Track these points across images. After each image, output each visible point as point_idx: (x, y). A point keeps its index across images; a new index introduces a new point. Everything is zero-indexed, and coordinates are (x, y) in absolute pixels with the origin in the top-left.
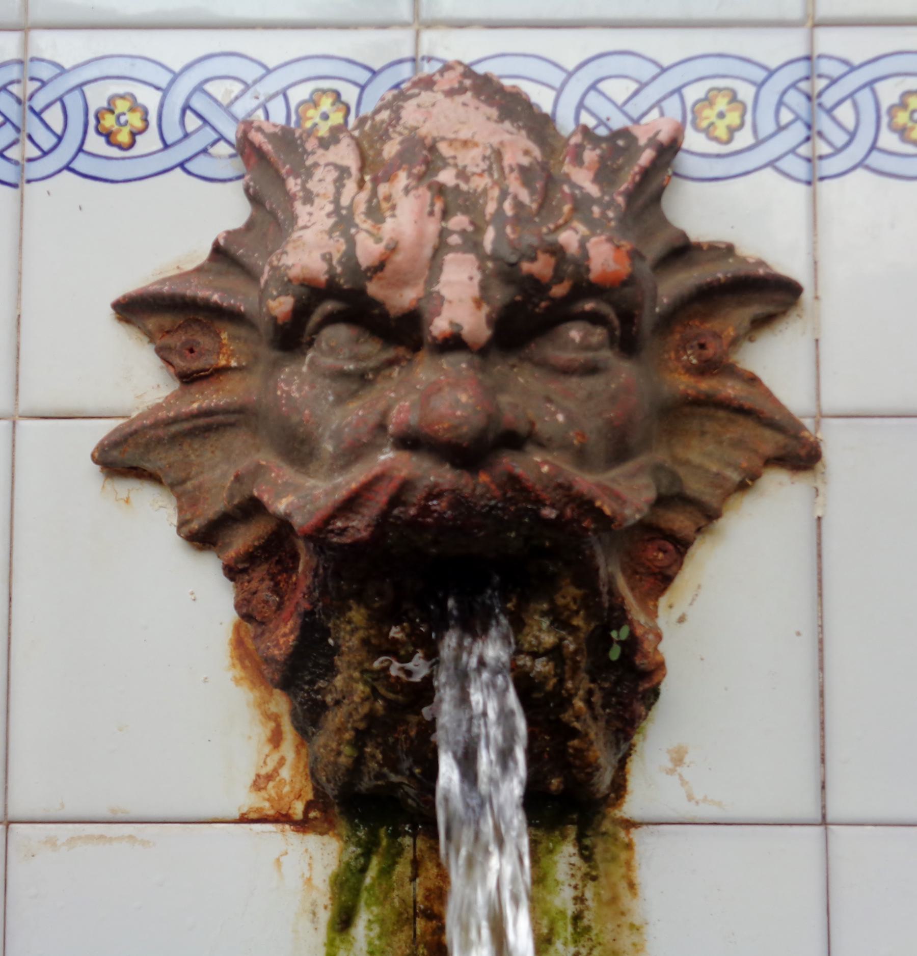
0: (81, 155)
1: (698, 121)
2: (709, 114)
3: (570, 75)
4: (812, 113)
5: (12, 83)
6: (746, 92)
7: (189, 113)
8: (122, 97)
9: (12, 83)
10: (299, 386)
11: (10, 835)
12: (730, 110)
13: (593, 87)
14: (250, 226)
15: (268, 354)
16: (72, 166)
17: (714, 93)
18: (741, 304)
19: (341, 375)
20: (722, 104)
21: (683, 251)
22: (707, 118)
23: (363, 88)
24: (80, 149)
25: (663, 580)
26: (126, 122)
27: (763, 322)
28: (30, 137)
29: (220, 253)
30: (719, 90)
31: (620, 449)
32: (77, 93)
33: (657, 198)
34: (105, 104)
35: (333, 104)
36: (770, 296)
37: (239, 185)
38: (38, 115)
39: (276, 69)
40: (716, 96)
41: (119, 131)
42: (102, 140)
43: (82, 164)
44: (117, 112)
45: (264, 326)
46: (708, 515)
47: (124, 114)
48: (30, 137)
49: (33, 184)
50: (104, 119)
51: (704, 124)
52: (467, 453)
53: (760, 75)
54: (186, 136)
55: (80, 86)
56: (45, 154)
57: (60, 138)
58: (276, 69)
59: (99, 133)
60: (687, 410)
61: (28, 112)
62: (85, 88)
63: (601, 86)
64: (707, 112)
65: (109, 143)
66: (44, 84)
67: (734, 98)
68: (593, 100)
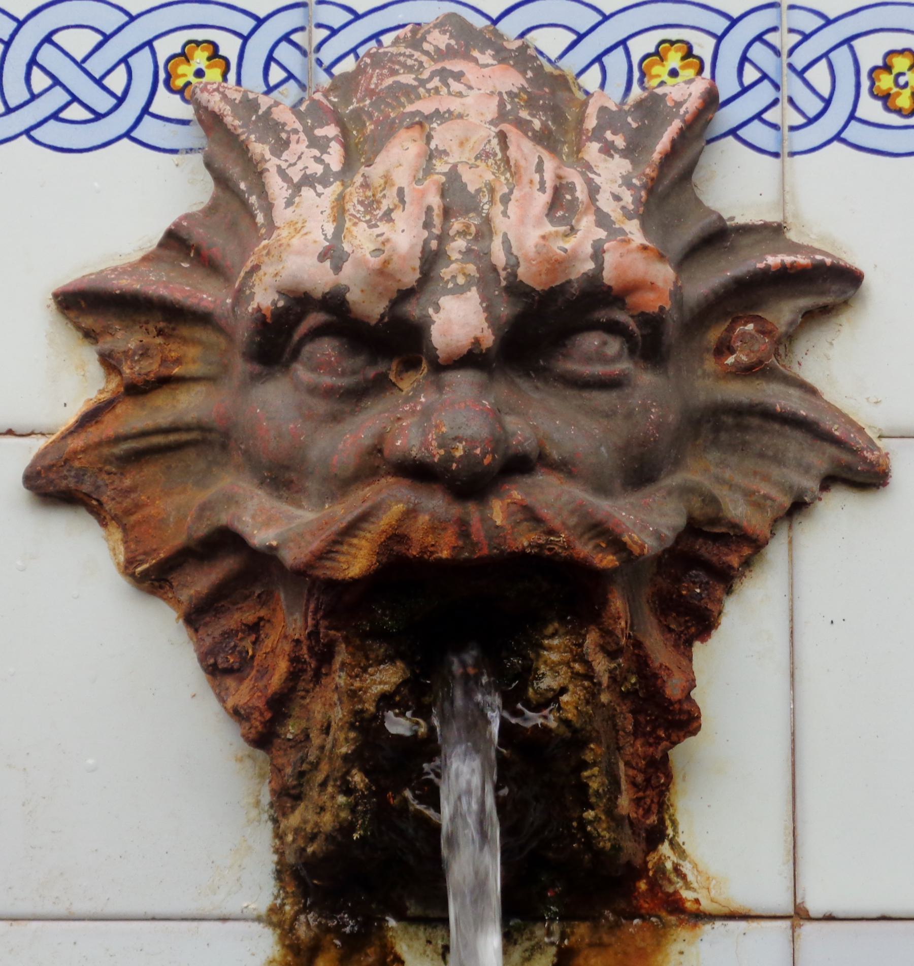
0: (853, 123)
1: (646, 80)
2: (186, 73)
3: (21, 24)
4: (308, 71)
5: (295, 31)
6: (229, 47)
7: (36, 70)
8: (902, 52)
9: (295, 31)
10: (276, 406)
11: (800, 943)
12: (684, 67)
13: (48, 39)
14: (212, 209)
15: (241, 367)
16: (843, 135)
17: (667, 45)
18: (793, 296)
19: (329, 393)
20: (200, 58)
21: (719, 237)
22: (184, 75)
23: (246, 39)
24: (852, 117)
25: (703, 623)
26: (906, 85)
27: (816, 316)
28: (791, 101)
29: (176, 241)
30: (198, 43)
31: (640, 470)
32: (845, 48)
33: (687, 175)
34: (880, 63)
35: (684, 58)
36: (829, 287)
37: (197, 159)
38: (801, 74)
39: (613, 15)
40: (669, 50)
41: (898, 94)
42: (879, 104)
43: (855, 132)
44: (895, 71)
45: (243, 332)
46: (753, 546)
47: (902, 74)
48: (791, 101)
49: (797, 157)
50: (880, 80)
51: (179, 83)
52: (466, 483)
53: (720, 25)
54: (34, 97)
55: (848, 41)
56: (811, 121)
57: (828, 102)
58: (613, 15)
59: (875, 96)
60: (755, 422)
61: (786, 70)
62: (855, 43)
63: (55, 38)
64: (656, 70)
65: (887, 109)
66: (334, 32)
67: (215, 53)
68: (47, 55)
